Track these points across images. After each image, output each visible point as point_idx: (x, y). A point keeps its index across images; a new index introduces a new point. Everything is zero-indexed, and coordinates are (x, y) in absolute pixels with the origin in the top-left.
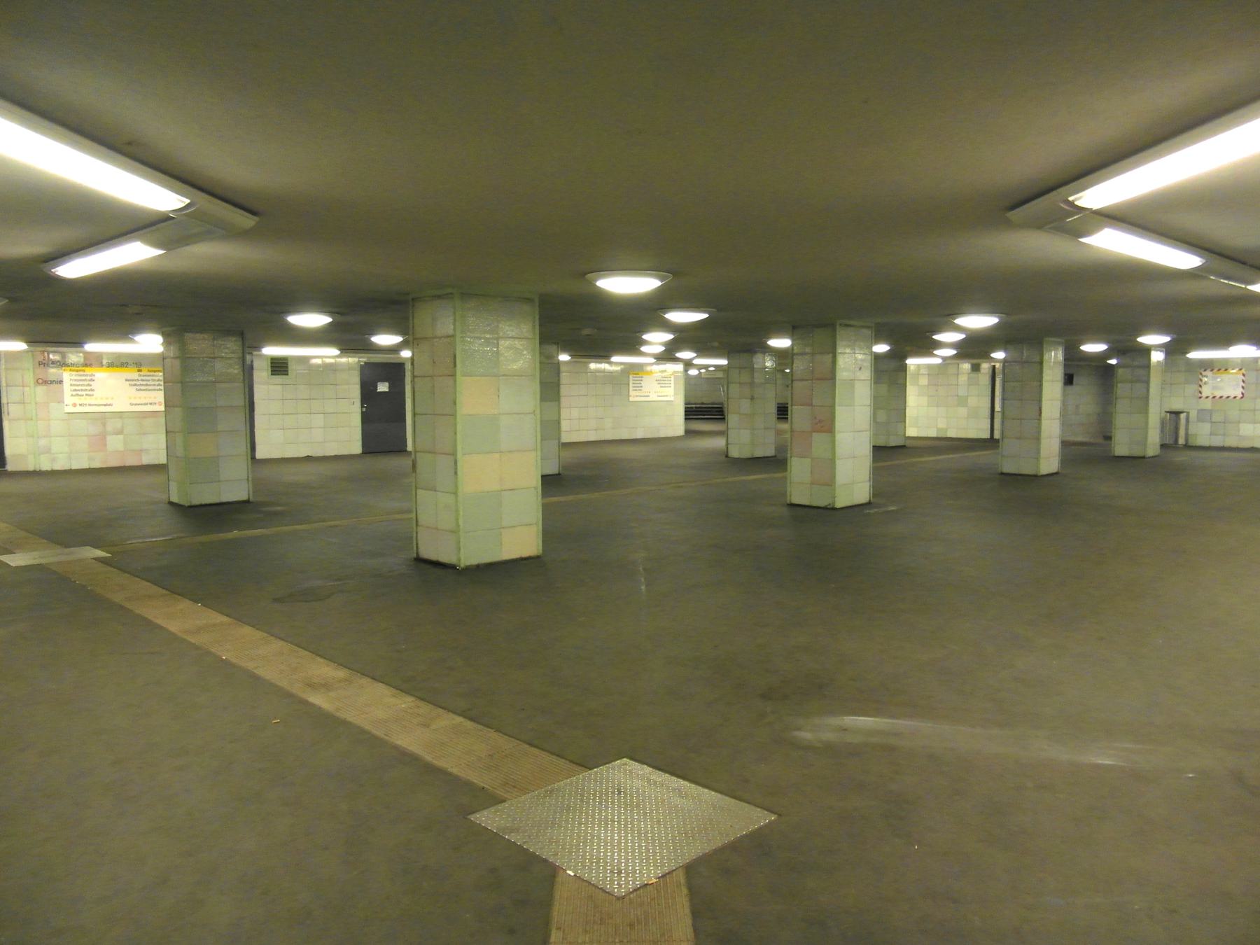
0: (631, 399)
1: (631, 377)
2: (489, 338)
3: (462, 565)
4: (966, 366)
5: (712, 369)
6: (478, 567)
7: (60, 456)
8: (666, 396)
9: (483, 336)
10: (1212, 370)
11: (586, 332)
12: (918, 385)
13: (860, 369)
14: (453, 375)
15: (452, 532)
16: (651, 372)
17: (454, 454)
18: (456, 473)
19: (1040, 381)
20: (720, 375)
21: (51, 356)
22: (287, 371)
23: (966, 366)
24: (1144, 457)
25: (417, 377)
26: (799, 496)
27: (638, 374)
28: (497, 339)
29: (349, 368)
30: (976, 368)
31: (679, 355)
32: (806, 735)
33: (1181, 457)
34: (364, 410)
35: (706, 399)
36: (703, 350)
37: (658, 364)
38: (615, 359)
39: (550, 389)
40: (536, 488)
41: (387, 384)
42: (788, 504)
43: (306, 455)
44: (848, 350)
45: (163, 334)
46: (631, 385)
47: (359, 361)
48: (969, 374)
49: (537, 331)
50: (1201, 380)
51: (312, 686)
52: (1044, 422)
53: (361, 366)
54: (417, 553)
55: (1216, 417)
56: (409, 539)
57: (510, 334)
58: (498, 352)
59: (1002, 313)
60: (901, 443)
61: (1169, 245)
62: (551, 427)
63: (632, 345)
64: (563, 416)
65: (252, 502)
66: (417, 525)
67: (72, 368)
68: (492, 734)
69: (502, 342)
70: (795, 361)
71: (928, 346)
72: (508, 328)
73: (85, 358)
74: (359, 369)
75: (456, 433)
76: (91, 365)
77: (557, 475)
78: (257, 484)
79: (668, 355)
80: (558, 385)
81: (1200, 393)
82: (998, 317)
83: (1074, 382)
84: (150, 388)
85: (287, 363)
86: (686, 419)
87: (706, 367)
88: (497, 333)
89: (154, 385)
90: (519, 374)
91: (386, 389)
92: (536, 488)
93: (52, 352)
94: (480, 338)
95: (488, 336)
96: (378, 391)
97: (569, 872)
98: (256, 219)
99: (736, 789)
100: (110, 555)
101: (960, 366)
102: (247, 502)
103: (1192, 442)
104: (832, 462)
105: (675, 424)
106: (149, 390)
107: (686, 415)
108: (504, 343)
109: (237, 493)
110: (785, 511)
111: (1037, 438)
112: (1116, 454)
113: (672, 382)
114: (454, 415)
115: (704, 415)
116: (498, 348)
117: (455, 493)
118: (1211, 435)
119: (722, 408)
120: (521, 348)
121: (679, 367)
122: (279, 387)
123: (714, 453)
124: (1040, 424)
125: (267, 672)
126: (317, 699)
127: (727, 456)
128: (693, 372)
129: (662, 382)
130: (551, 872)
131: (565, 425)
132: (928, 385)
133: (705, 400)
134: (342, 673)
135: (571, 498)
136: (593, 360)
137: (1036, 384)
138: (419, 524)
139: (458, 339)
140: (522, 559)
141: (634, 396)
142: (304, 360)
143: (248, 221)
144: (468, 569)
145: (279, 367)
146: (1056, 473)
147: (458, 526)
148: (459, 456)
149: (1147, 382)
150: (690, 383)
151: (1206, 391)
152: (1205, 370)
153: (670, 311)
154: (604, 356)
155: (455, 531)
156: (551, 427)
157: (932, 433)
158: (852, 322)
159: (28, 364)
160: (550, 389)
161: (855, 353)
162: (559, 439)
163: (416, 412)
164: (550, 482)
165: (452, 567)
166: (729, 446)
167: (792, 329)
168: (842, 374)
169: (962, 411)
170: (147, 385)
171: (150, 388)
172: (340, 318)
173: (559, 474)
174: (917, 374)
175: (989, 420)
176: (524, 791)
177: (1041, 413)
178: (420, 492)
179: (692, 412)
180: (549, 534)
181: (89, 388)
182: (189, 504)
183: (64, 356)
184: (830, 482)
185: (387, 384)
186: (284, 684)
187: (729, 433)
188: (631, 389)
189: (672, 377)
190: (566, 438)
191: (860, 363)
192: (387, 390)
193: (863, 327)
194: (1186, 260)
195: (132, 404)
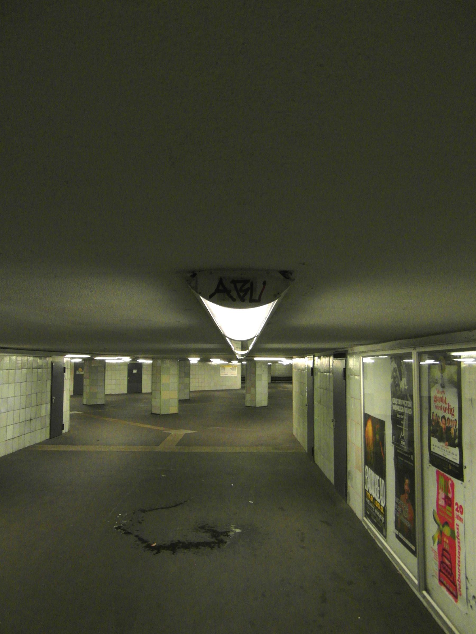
0: (221, 375)
7: (319, 373)
8: (234, 374)
26: (248, 404)
27: (223, 366)
34: (128, 379)
41: (136, 370)
43: (109, 393)
91: (136, 372)
102: (104, 404)
109: (100, 402)
113: (236, 369)
114: (160, 383)
141: (222, 374)
148: (161, 391)
155: (160, 407)
159: (404, 416)
165: (159, 414)
173: (189, 399)
175: (365, 388)
185: (136, 370)
188: (221, 371)
190: (191, 390)
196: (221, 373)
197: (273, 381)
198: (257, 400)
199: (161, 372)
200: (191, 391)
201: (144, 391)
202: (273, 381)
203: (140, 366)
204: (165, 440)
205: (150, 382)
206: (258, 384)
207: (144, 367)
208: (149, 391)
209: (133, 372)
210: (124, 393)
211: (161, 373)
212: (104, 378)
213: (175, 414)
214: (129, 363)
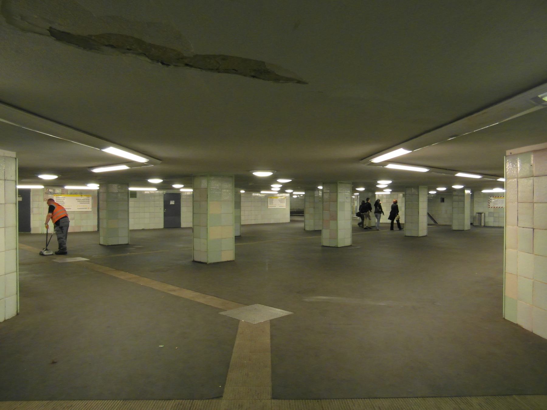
0: (269, 207)
1: (269, 199)
3: (209, 263)
8: (283, 206)
10: (493, 197)
14: (207, 201)
15: (206, 252)
16: (277, 197)
17: (207, 226)
18: (207, 233)
19: (418, 201)
21: (50, 190)
22: (136, 196)
24: (463, 230)
25: (195, 201)
26: (326, 243)
27: (271, 198)
28: (221, 189)
29: (159, 195)
31: (286, 191)
32: (307, 300)
33: (478, 230)
34: (165, 211)
35: (299, 207)
36: (295, 189)
37: (279, 194)
38: (262, 192)
39: (238, 205)
40: (233, 238)
41: (174, 201)
42: (322, 246)
45: (100, 184)
46: (269, 202)
47: (163, 193)
50: (489, 201)
52: (420, 217)
53: (164, 195)
54: (193, 259)
55: (495, 215)
61: (410, 166)
62: (238, 218)
64: (242, 214)
65: (130, 245)
66: (194, 250)
67: (57, 195)
73: (62, 191)
75: (207, 220)
76: (64, 194)
77: (239, 236)
79: (282, 191)
80: (240, 202)
81: (489, 205)
82: (392, 181)
83: (445, 201)
84: (85, 202)
85: (136, 193)
86: (290, 215)
87: (300, 195)
89: (87, 201)
93: (50, 189)
96: (170, 204)
98: (161, 161)
101: (399, 195)
102: (128, 244)
103: (487, 225)
105: (286, 217)
106: (85, 203)
107: (290, 214)
109: (123, 240)
111: (418, 223)
112: (454, 229)
113: (285, 201)
114: (207, 214)
117: (207, 239)
118: (494, 222)
119: (304, 211)
124: (418, 218)
126: (171, 293)
127: (305, 230)
129: (281, 201)
131: (243, 218)
134: (177, 288)
135: (244, 244)
138: (194, 249)
141: (270, 206)
142: (141, 192)
143: (160, 162)
144: (211, 264)
145: (134, 194)
146: (426, 236)
148: (208, 226)
149: (464, 202)
150: (292, 201)
151: (491, 205)
152: (491, 197)
153: (279, 179)
154: (258, 191)
156: (238, 218)
160: (238, 205)
162: (240, 223)
164: (238, 239)
165: (205, 263)
166: (306, 226)
167: (323, 184)
170: (84, 201)
171: (85, 202)
172: (165, 180)
173: (240, 236)
177: (419, 213)
178: (195, 239)
179: (293, 213)
180: (236, 255)
181: (63, 202)
182: (108, 245)
183: (54, 190)
187: (306, 221)
188: (269, 203)
189: (285, 199)
190: (242, 224)
192: (174, 204)
194: (424, 170)
195: (78, 209)
198: (339, 238)
199: (207, 195)
200: (242, 225)
201: (183, 225)
203: (177, 196)
206: (340, 214)
207: (183, 198)
208: (190, 225)
211: (207, 198)
214: (165, 193)
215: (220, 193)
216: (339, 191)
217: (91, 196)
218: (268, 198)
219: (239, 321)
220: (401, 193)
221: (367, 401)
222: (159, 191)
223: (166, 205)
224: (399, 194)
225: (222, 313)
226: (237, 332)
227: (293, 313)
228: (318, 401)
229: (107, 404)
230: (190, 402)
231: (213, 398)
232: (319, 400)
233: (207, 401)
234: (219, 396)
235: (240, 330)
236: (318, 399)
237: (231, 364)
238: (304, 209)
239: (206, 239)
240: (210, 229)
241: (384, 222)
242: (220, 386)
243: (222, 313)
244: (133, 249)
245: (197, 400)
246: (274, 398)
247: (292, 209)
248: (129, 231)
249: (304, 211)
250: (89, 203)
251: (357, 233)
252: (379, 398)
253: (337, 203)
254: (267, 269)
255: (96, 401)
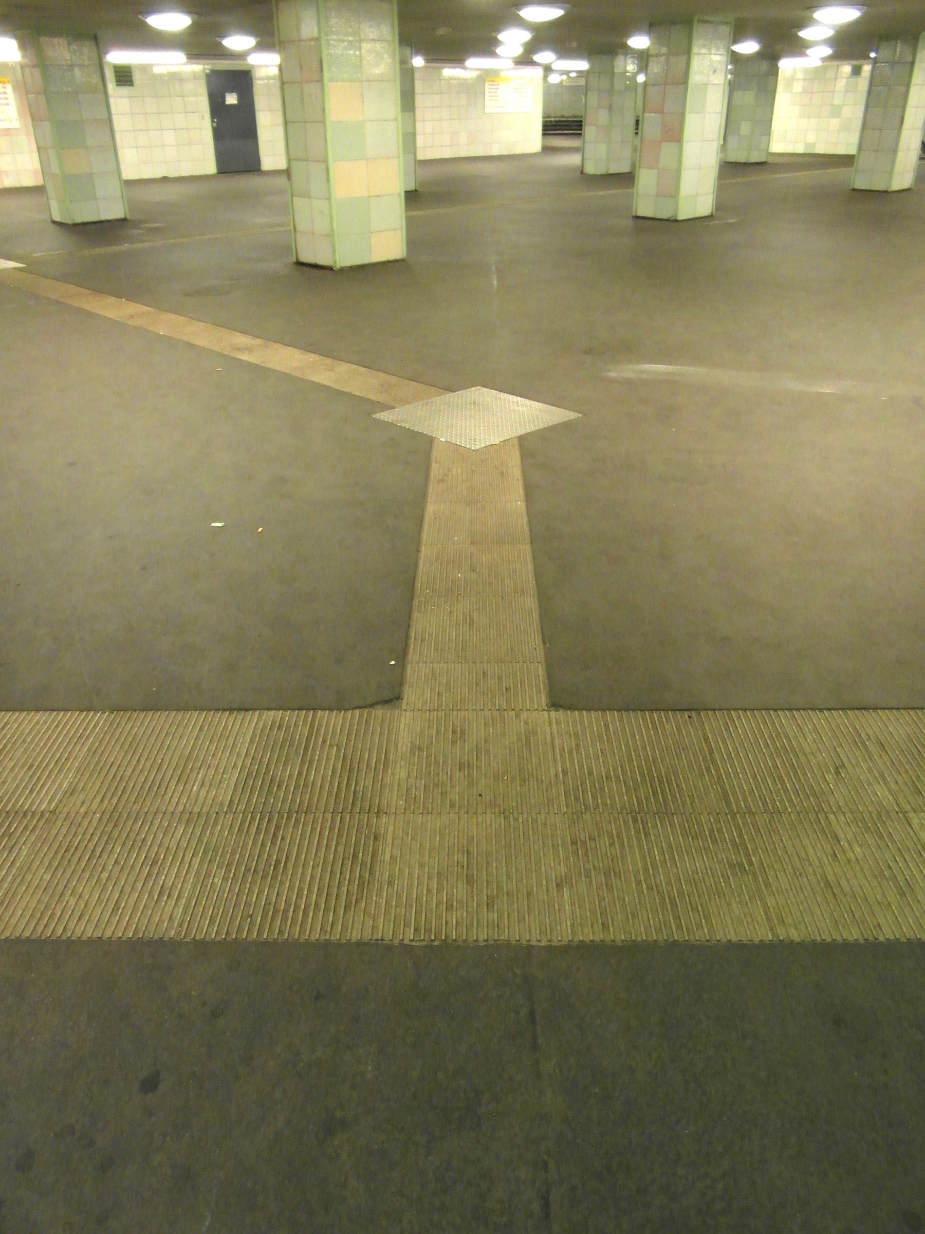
0: (487, 111)
1: (487, 84)
2: (352, 41)
4: (847, 69)
5: (573, 75)
6: (352, 269)
9: (346, 38)
11: (441, 31)
12: (791, 92)
13: (715, 71)
14: (321, 80)
17: (325, 160)
18: (328, 180)
19: (908, 86)
20: (582, 82)
23: (847, 69)
26: (645, 209)
27: (494, 81)
28: (360, 41)
29: (195, 77)
30: (857, 71)
32: (613, 374)
34: (215, 125)
35: (567, 112)
36: (564, 52)
37: (516, 69)
40: (399, 195)
44: (704, 51)
46: (487, 94)
47: (204, 69)
48: (847, 78)
49: (397, 31)
51: (238, 349)
54: (297, 258)
56: (288, 249)
57: (371, 36)
58: (360, 56)
59: (857, 5)
60: (764, 160)
62: (409, 140)
63: (487, 46)
68: (381, 374)
69: (364, 45)
70: (650, 64)
71: (798, 47)
72: (370, 30)
74: (205, 78)
77: (413, 191)
78: (131, 204)
79: (525, 60)
82: (859, 10)
85: (130, 72)
87: (567, 73)
88: (359, 36)
90: (380, 79)
92: (399, 195)
94: (343, 41)
95: (351, 39)
97: (441, 439)
99: (556, 401)
100: (24, 265)
102: (124, 220)
104: (677, 175)
108: (366, 46)
109: (113, 210)
110: (630, 223)
114: (323, 122)
115: (563, 130)
116: (360, 51)
119: (581, 121)
120: (382, 51)
121: (539, 71)
122: (126, 101)
123: (568, 169)
125: (201, 342)
126: (245, 357)
127: (582, 173)
128: (554, 79)
130: (430, 441)
132: (803, 92)
133: (566, 113)
134: (259, 341)
136: (448, 65)
137: (902, 89)
138: (297, 229)
139: (323, 42)
140: (389, 262)
141: (490, 106)
142: (145, 68)
144: (342, 270)
145: (124, 76)
147: (332, 230)
150: (550, 93)
155: (331, 235)
156: (409, 140)
157: (800, 149)
158: (709, 18)
161: (711, 54)
163: (287, 120)
164: (412, 197)
165: (330, 269)
167: (652, 26)
168: (695, 78)
169: (835, 123)
173: (416, 190)
174: (791, 80)
176: (410, 403)
177: (902, 122)
179: (552, 127)
180: (412, 243)
182: (72, 222)
184: (674, 194)
186: (217, 348)
190: (421, 156)
191: (715, 65)
193: (723, 23)
196: (487, 103)
197: (547, 132)
202: (547, 132)
204: (337, 81)
205: (280, 132)
208: (282, 165)
209: (224, 101)
210: (208, 173)
212: (106, 116)
213: (396, 261)
214: (208, 71)
215: (358, 53)
216: (695, 50)
217: (9, 82)
218: (484, 81)
219: (431, 440)
220: (846, 62)
221: (839, 717)
222: (192, 64)
223: (217, 107)
224: (842, 65)
225: (384, 416)
226: (427, 476)
227: (580, 415)
228: (690, 717)
229: (66, 723)
230: (306, 717)
231: (372, 706)
232: (694, 714)
233: (357, 712)
234: (392, 699)
235: (436, 470)
236: (691, 709)
237: (418, 584)
238: (582, 117)
239: (327, 199)
240: (338, 169)
241: (786, 152)
242: (393, 663)
243: (384, 416)
244: (140, 231)
245: (325, 710)
246: (554, 705)
247: (547, 117)
248: (123, 184)
249: (581, 121)
250: (8, 104)
251: (727, 181)
252: (875, 709)
253: (686, 89)
254: (495, 283)
255: (33, 713)
